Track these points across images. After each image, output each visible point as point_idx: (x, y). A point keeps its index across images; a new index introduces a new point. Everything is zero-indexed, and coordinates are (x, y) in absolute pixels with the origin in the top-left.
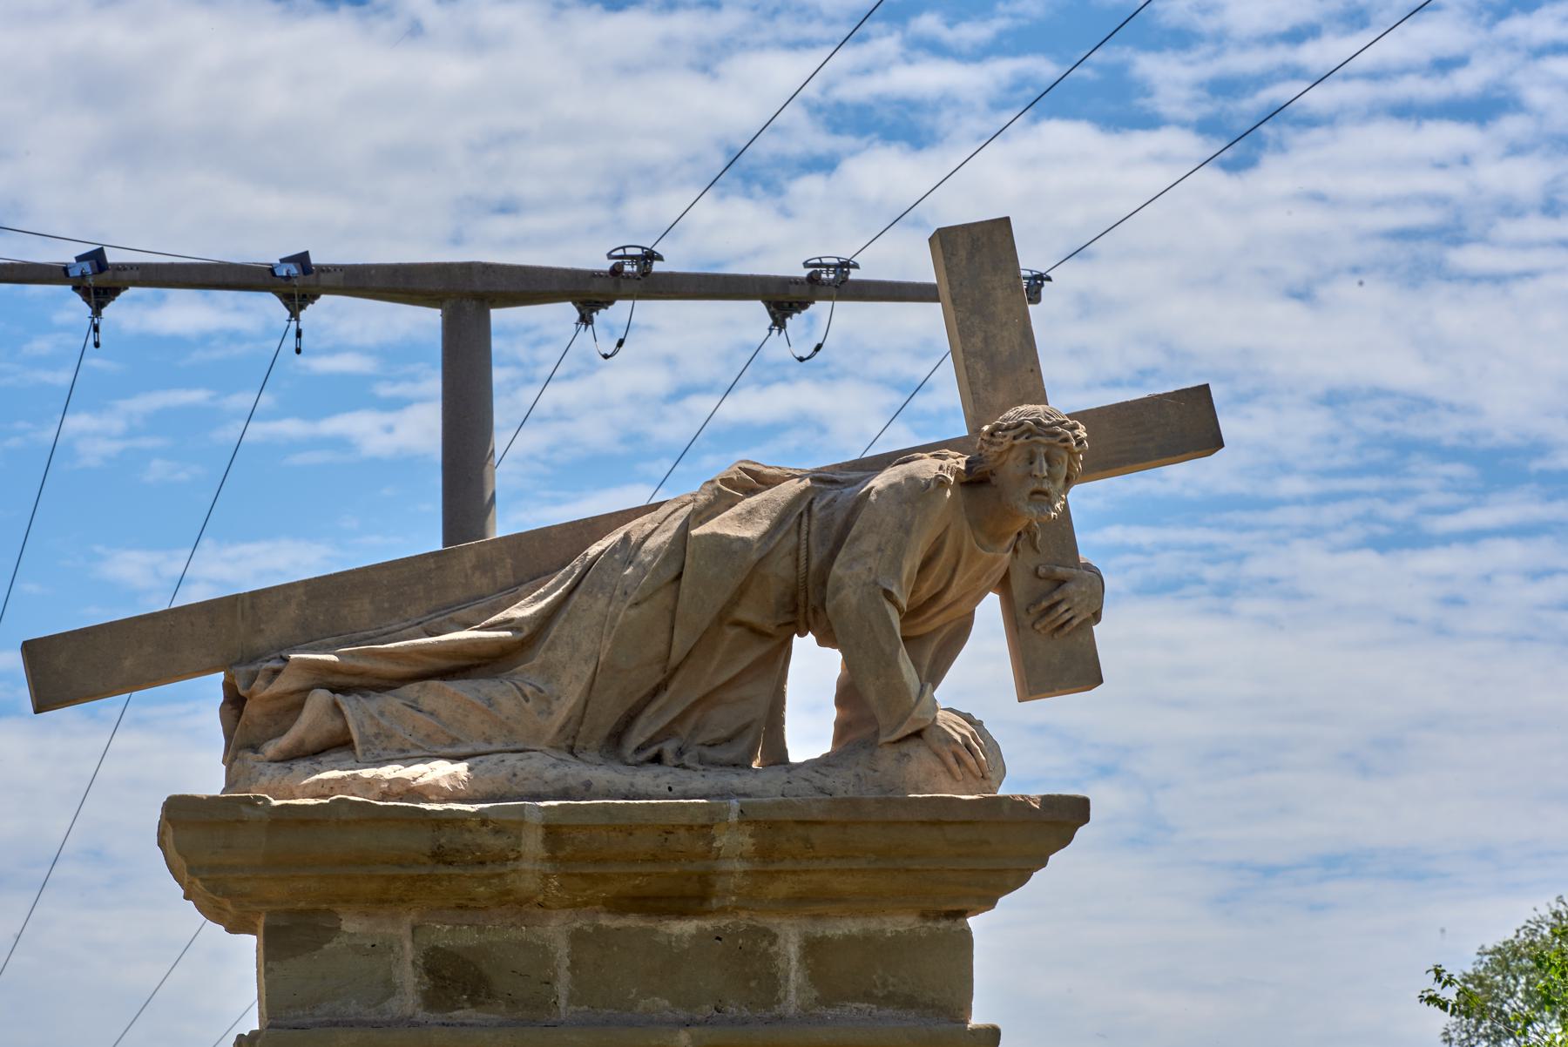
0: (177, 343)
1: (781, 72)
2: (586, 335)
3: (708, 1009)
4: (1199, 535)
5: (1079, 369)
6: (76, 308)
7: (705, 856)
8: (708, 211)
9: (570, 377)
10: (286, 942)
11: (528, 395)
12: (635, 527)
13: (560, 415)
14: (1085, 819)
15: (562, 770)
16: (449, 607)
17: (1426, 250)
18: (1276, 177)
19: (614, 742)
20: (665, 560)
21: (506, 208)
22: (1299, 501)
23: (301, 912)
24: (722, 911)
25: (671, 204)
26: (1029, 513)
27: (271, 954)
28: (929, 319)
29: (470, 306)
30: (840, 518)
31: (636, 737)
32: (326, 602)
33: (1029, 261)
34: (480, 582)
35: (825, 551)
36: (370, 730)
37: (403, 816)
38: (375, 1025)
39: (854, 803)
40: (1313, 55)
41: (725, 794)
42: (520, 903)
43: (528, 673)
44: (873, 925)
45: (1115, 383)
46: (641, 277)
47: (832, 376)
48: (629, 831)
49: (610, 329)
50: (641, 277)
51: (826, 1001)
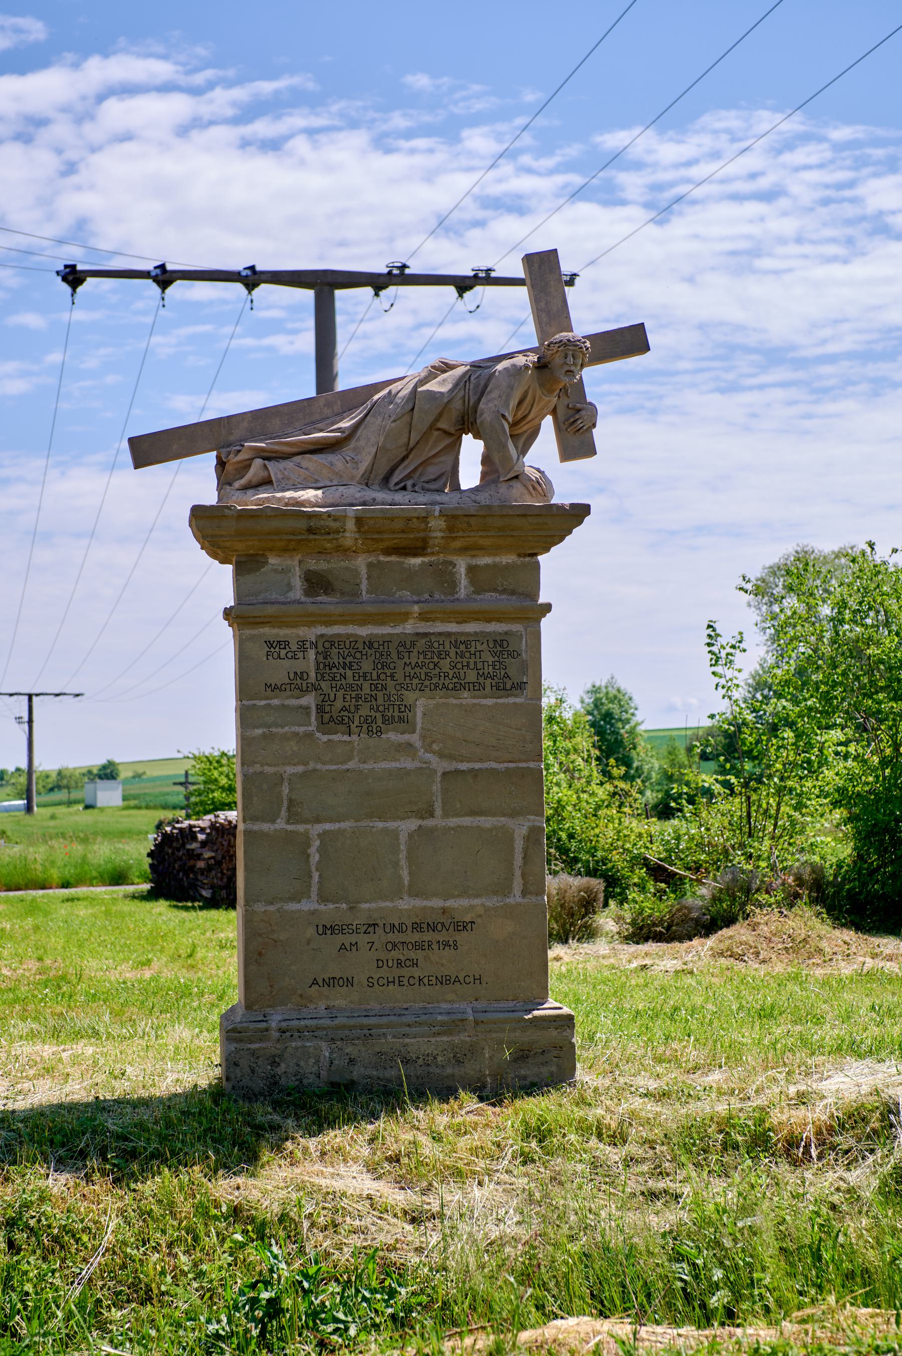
0: (198, 305)
1: (463, 182)
2: (377, 301)
3: (426, 596)
4: (643, 387)
5: (588, 315)
6: (155, 289)
7: (424, 530)
8: (430, 244)
9: (370, 320)
10: (245, 567)
11: (352, 328)
12: (394, 387)
13: (366, 336)
14: (589, 513)
15: (363, 493)
16: (314, 423)
17: (744, 259)
18: (679, 227)
19: (386, 481)
20: (407, 401)
21: (343, 244)
22: (686, 372)
23: (251, 555)
24: (433, 554)
25: (415, 241)
26: (565, 380)
27: (239, 572)
28: (522, 293)
29: (326, 289)
30: (482, 383)
31: (395, 478)
32: (261, 419)
33: (566, 267)
34: (327, 411)
35: (476, 397)
36: (280, 476)
37: (294, 513)
38: (284, 603)
39: (489, 507)
40: (696, 172)
41: (433, 503)
42: (346, 551)
43: (348, 451)
44: (497, 559)
45: (607, 321)
46: (400, 276)
47: (484, 318)
48: (392, 519)
49: (388, 297)
50: (400, 276)
51: (477, 592)
